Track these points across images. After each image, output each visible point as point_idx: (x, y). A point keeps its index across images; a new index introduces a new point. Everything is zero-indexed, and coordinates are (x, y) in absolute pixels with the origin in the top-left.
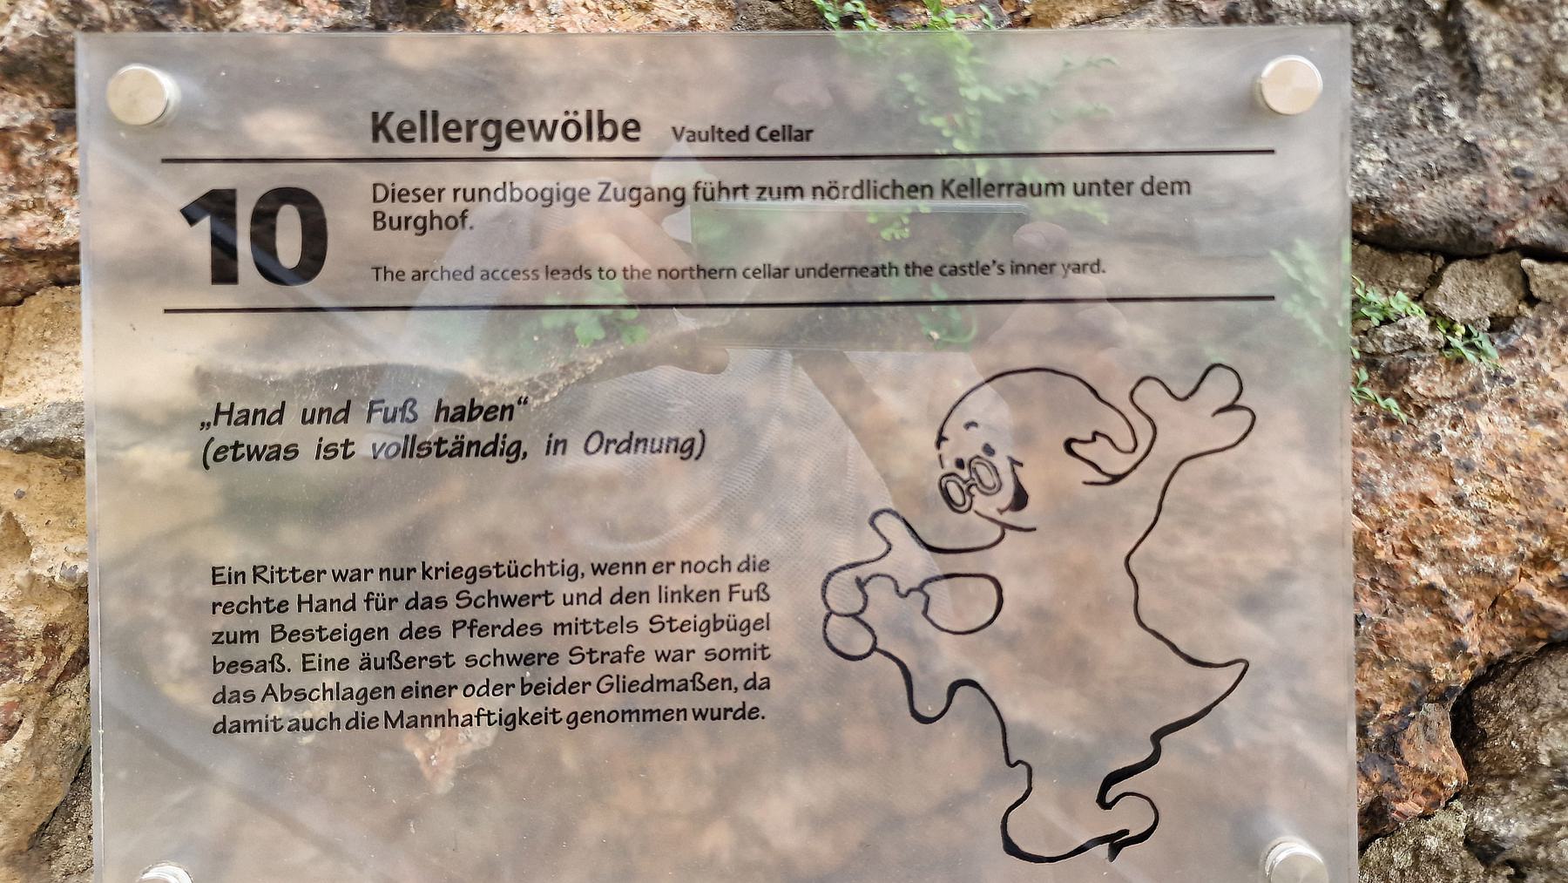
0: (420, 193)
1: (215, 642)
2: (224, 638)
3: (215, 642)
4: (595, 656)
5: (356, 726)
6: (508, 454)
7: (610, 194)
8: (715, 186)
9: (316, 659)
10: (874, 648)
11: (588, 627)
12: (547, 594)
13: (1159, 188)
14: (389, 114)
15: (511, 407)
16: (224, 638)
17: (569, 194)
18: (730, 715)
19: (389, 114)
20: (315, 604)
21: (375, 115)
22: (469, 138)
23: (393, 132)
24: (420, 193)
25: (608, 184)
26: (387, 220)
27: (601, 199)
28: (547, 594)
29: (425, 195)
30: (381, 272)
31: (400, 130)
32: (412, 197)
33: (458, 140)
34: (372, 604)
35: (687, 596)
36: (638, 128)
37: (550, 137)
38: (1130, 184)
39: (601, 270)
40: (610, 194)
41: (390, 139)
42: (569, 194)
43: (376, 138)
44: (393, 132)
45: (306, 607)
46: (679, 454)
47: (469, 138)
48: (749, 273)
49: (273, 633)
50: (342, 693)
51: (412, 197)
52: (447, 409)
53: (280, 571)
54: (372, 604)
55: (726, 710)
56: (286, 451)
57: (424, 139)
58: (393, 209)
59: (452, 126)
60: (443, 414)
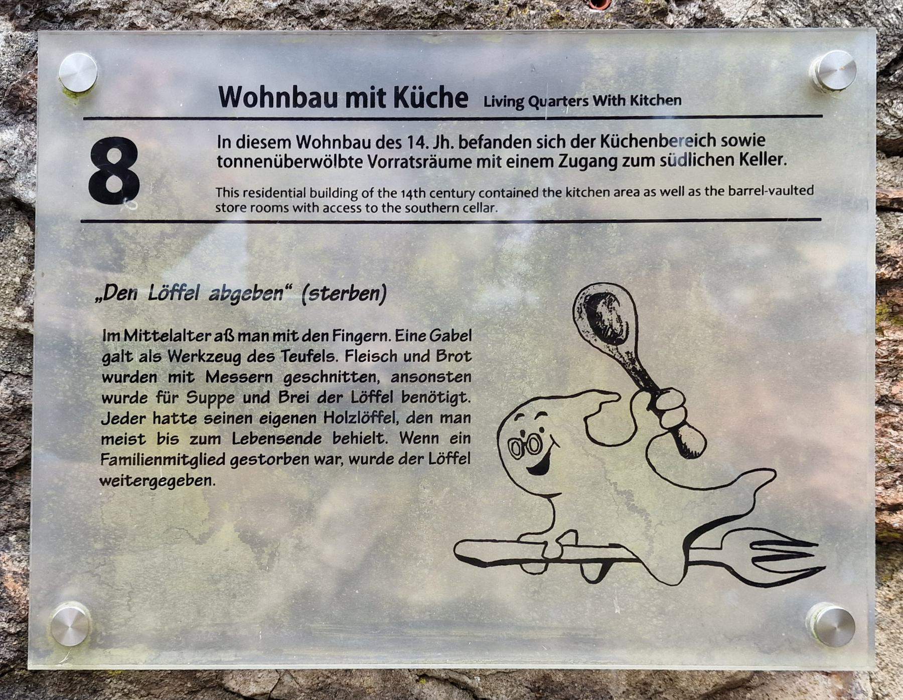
0: (266, 142)
2: (197, 440)
6: (235, 361)
7: (566, 163)
8: (413, 197)
9: (404, 333)
13: (388, 143)
14: (406, 88)
15: (281, 291)
16: (197, 440)
19: (406, 88)
21: (397, 88)
23: (748, 161)
24: (266, 142)
25: (566, 155)
27: (561, 166)
29: (269, 143)
31: (751, 160)
34: (162, 398)
35: (201, 358)
36: (466, 99)
37: (235, 104)
38: (593, 140)
39: (367, 206)
40: (566, 163)
41: (406, 106)
42: (583, 162)
43: (397, 106)
44: (748, 161)
46: (272, 424)
48: (341, 209)
51: (261, 145)
52: (159, 417)
54: (162, 398)
57: (761, 164)
59: (462, 96)
60: (157, 419)
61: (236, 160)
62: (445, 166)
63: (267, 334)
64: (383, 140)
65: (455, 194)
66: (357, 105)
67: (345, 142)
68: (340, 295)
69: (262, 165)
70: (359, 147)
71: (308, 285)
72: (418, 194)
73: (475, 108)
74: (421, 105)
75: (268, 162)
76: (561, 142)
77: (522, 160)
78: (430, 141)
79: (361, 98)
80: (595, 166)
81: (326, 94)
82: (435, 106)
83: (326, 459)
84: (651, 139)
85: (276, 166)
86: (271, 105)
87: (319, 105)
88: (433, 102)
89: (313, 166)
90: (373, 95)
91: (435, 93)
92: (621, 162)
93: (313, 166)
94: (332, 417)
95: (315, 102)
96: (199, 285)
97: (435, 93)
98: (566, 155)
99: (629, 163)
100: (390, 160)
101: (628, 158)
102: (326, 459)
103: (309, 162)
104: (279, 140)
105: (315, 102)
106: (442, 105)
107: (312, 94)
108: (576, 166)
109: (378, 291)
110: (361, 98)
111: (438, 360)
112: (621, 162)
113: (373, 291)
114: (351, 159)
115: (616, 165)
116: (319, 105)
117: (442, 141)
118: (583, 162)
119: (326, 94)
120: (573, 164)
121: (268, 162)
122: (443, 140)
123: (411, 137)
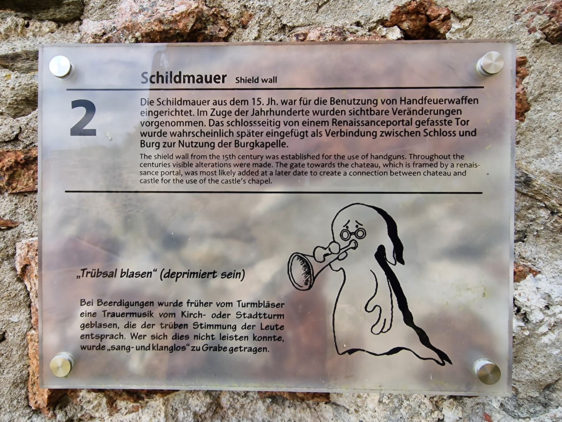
1: (192, 350)
2: (195, 348)
3: (192, 350)
4: (242, 349)
5: (128, 327)
7: (215, 113)
10: (334, 241)
11: (261, 316)
12: (215, 272)
15: (151, 272)
16: (195, 348)
17: (448, 112)
18: (95, 348)
20: (407, 101)
22: (457, 114)
25: (214, 109)
26: (145, 143)
28: (215, 272)
30: (412, 156)
32: (364, 123)
33: (219, 82)
42: (224, 113)
45: (403, 102)
47: (457, 114)
49: (98, 302)
50: (98, 325)
51: (364, 123)
53: (260, 314)
55: (93, 346)
56: (136, 274)
58: (148, 140)
61: (295, 122)
62: (279, 115)
63: (242, 307)
64: (234, 101)
65: (252, 157)
66: (163, 82)
67: (182, 102)
68: (207, 275)
69: (340, 103)
70: (195, 104)
71: (164, 269)
72: (231, 157)
73: (230, 82)
74: (211, 82)
75: (344, 101)
76: (231, 134)
77: (311, 122)
78: (265, 101)
79: (191, 78)
80: (352, 125)
81: (206, 76)
82: (154, 83)
83: (177, 133)
84: (431, 111)
85: (348, 104)
86: (163, 82)
87: (202, 82)
88: (153, 81)
89: (450, 103)
90: (167, 76)
91: (154, 76)
92: (379, 134)
93: (450, 103)
94: (405, 100)
95: (200, 80)
96: (116, 270)
97: (154, 76)
98: (214, 109)
99: (166, 145)
100: (152, 122)
101: (166, 143)
102: (177, 133)
103: (447, 101)
104: (242, 101)
105: (200, 80)
106: (158, 82)
107: (198, 76)
108: (298, 136)
109: (240, 273)
110: (191, 78)
111: (98, 305)
112: (379, 134)
113: (148, 273)
114: (182, 111)
115: (376, 136)
116: (202, 82)
117: (271, 101)
118: (224, 113)
119: (206, 76)
120: (218, 114)
121: (344, 101)
122: (272, 101)
123: (254, 99)
